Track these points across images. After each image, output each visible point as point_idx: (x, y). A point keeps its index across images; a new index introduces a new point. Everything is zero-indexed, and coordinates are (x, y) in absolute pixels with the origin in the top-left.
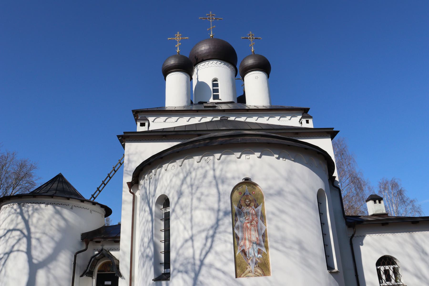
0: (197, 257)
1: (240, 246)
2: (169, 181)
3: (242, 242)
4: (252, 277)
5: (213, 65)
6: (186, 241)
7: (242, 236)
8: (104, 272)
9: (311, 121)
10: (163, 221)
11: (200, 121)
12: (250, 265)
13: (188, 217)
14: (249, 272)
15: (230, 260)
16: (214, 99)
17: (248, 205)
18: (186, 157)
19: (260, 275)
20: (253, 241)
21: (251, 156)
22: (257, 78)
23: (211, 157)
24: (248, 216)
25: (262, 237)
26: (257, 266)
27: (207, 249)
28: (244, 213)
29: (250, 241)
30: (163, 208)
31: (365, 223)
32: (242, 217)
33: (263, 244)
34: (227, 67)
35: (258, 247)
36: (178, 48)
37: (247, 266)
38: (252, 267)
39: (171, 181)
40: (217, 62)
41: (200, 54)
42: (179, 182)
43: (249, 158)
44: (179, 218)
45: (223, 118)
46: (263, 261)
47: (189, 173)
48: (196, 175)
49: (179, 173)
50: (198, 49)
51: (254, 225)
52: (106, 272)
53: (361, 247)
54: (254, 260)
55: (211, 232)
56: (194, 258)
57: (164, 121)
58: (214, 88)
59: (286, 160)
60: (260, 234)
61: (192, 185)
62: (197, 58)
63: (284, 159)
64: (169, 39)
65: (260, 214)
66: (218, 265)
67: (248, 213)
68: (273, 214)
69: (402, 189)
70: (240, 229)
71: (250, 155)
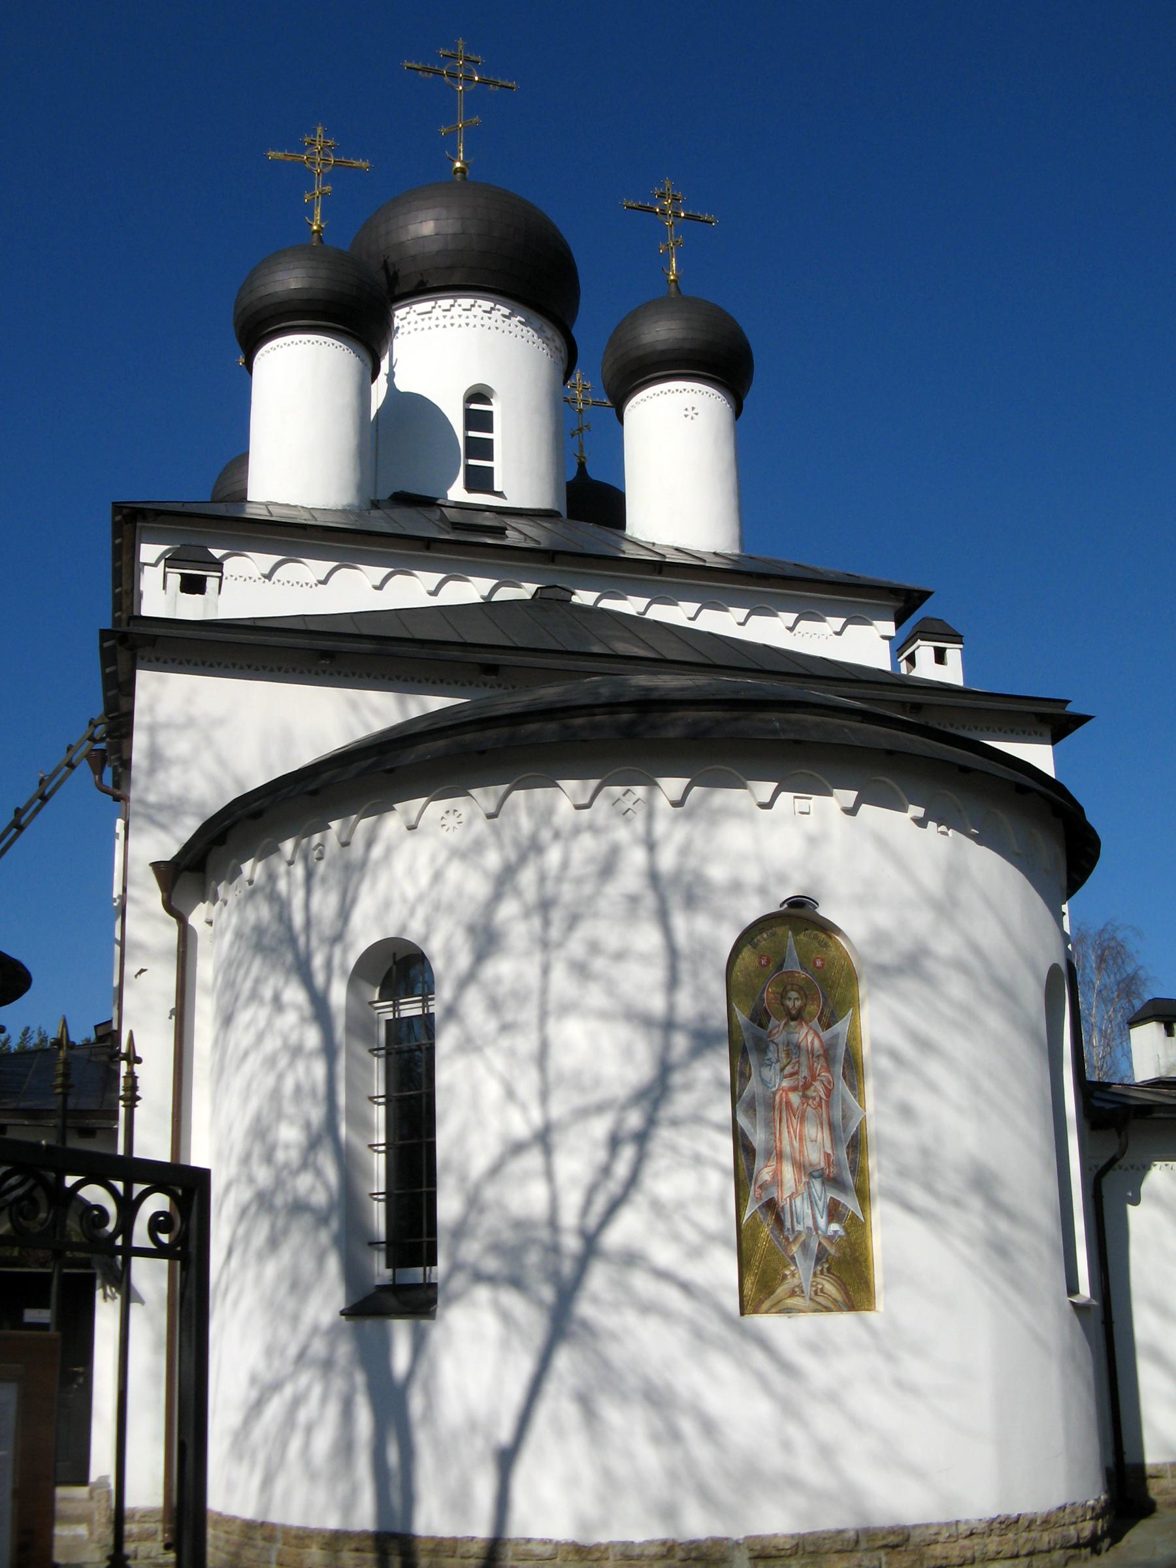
0: (569, 1217)
1: (759, 1183)
2: (424, 879)
3: (766, 1170)
4: (803, 1312)
5: (472, 321)
6: (517, 1148)
7: (767, 1142)
8: (22, 1266)
9: (954, 654)
10: (378, 1056)
11: (434, 593)
12: (796, 1266)
13: (526, 1044)
14: (793, 1294)
15: (712, 1238)
16: (470, 487)
17: (794, 1012)
18: (520, 777)
19: (832, 1306)
20: (811, 1165)
21: (816, 800)
22: (690, 413)
23: (640, 791)
24: (793, 1061)
25: (848, 1153)
26: (825, 1270)
27: (614, 1186)
28: (777, 1044)
29: (800, 1166)
30: (381, 1000)
31: (1161, 1115)
32: (768, 1062)
33: (849, 1178)
34: (536, 336)
35: (832, 1194)
36: (318, 212)
37: (786, 1266)
38: (802, 1272)
39: (438, 877)
40: (492, 309)
41: (413, 256)
42: (477, 887)
43: (808, 811)
44: (478, 1049)
45: (549, 594)
46: (848, 1250)
47: (533, 848)
48: (565, 864)
49: (478, 847)
50: (407, 226)
51: (818, 1099)
52: (29, 1267)
53: (1131, 1209)
54: (812, 1245)
55: (634, 1120)
56: (553, 1223)
57: (267, 572)
58: (472, 434)
59: (950, 832)
60: (841, 1137)
61: (545, 906)
62: (396, 273)
63: (943, 828)
64: (272, 155)
65: (841, 1052)
66: (664, 1255)
67: (794, 1049)
68: (895, 1055)
69: (1138, 972)
70: (761, 1112)
71: (810, 799)
